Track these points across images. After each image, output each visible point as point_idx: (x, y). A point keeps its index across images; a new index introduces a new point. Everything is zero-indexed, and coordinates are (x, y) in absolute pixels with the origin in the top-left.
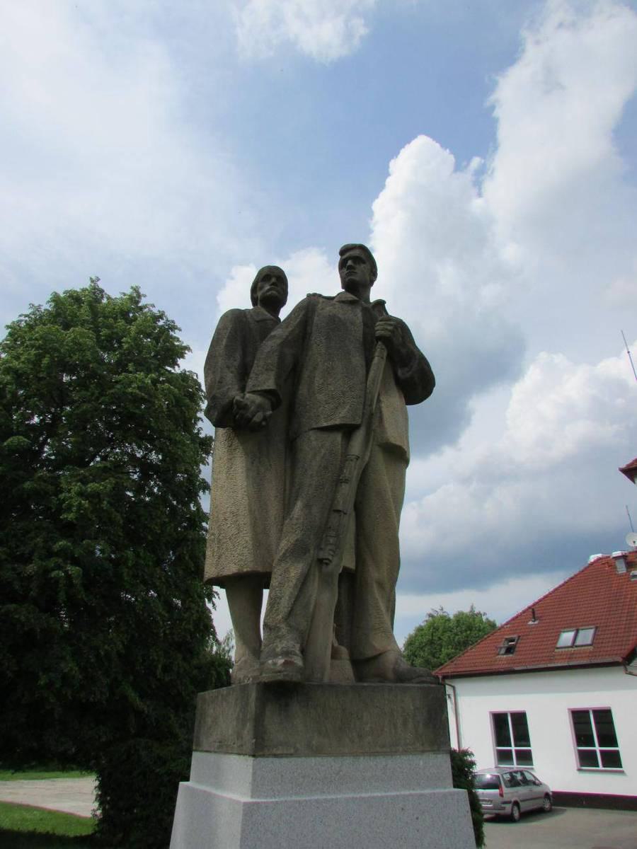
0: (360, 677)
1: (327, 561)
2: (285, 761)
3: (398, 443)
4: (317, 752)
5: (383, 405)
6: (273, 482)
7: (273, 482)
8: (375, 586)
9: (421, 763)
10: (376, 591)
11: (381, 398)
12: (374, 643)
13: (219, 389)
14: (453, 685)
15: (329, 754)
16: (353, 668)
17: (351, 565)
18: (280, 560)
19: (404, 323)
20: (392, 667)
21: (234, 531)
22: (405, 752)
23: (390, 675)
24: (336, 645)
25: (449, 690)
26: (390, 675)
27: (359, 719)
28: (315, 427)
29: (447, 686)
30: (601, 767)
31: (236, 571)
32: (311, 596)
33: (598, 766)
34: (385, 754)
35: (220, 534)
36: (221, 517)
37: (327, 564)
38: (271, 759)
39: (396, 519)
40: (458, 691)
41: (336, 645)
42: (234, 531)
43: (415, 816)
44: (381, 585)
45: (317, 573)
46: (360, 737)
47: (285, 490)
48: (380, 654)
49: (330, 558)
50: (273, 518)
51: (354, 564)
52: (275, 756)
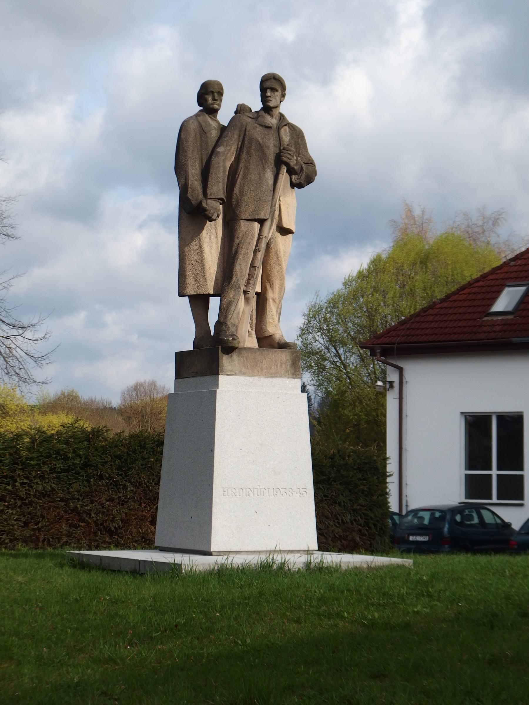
0: (260, 345)
2: (231, 377)
4: (244, 374)
11: (281, 199)
15: (249, 375)
16: (310, 157)
17: (259, 291)
22: (281, 377)
23: (276, 345)
24: (250, 330)
30: (495, 500)
33: (490, 498)
34: (272, 377)
38: (226, 376)
45: (243, 297)
46: (262, 370)
52: (227, 375)
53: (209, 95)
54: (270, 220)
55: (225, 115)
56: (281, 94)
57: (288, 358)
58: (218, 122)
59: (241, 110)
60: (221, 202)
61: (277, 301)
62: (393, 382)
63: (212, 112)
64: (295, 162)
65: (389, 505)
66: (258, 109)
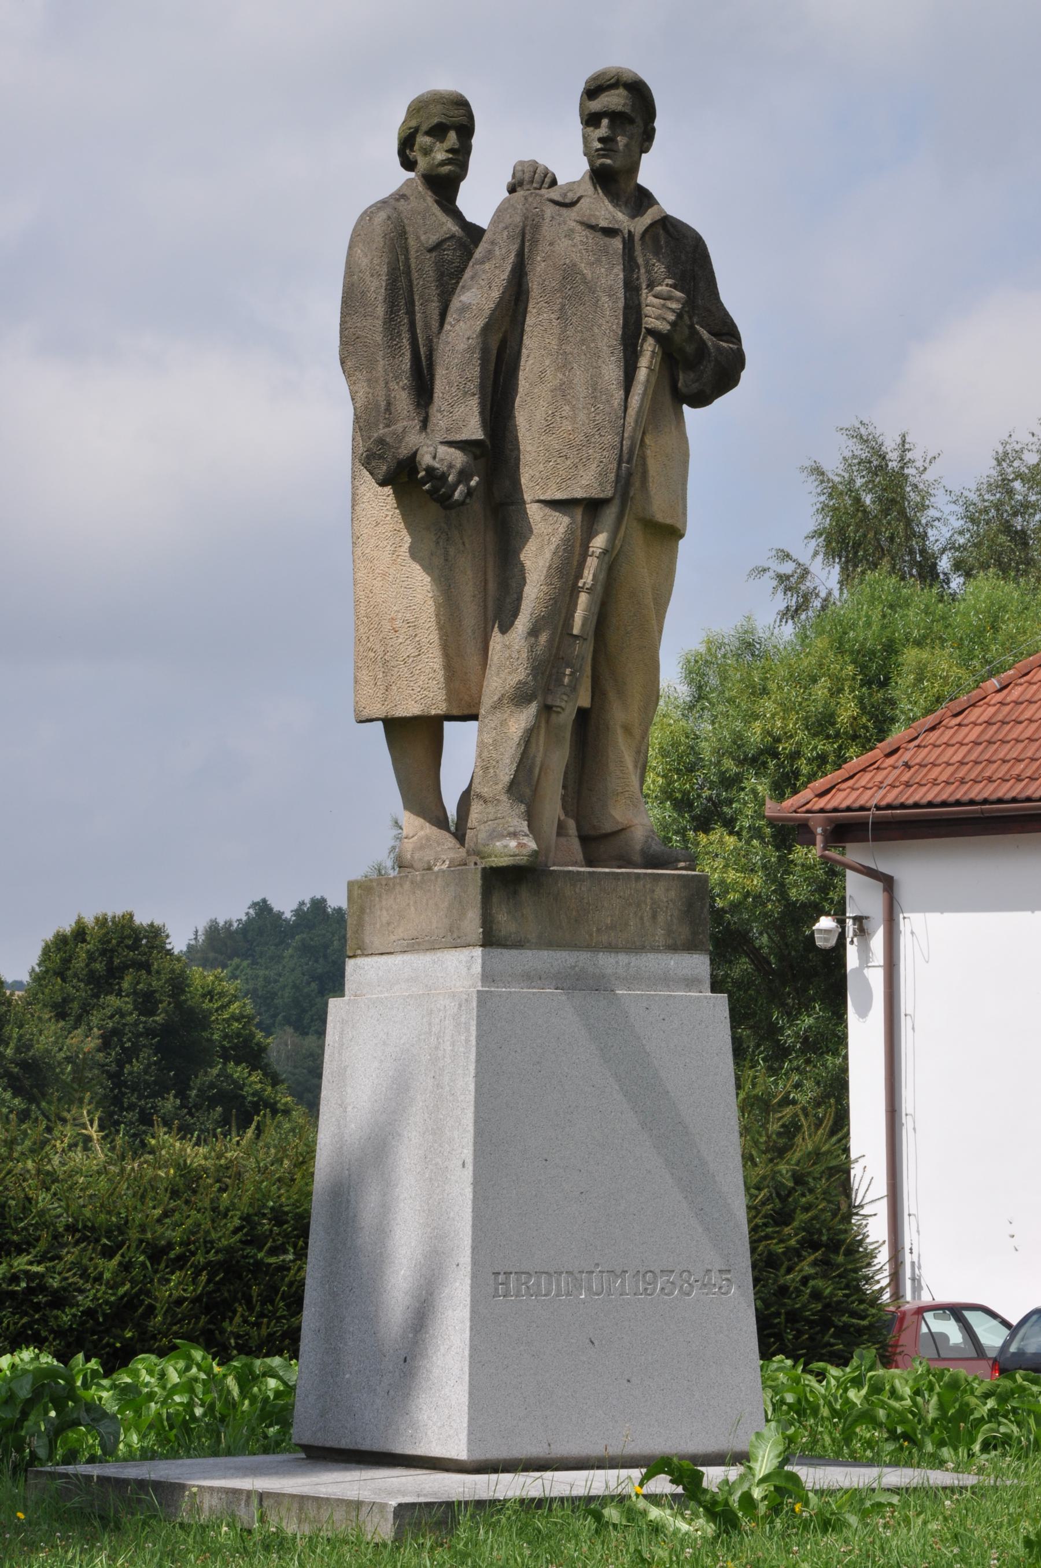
1: (559, 709)
3: (669, 521)
5: (648, 452)
6: (469, 572)
7: (469, 572)
8: (619, 731)
9: (672, 963)
10: (620, 740)
11: (647, 441)
12: (613, 813)
13: (388, 426)
14: (884, 868)
18: (494, 708)
19: (701, 238)
20: (638, 847)
21: (411, 650)
23: (637, 858)
24: (562, 818)
25: (861, 895)
26: (637, 858)
27: (864, 747)
28: (542, 498)
29: (852, 878)
31: (419, 713)
32: (535, 757)
35: (385, 653)
36: (387, 626)
37: (559, 713)
39: (657, 634)
40: (905, 891)
41: (562, 818)
42: (411, 650)
43: (662, 1017)
44: (627, 730)
47: (486, 582)
48: (623, 829)
49: (563, 704)
50: (469, 631)
51: (589, 700)
53: (439, 135)
54: (617, 502)
55: (481, 198)
56: (641, 130)
57: (672, 894)
58: (457, 215)
59: (531, 180)
60: (478, 452)
61: (637, 732)
62: (867, 918)
63: (444, 186)
64: (687, 331)
65: (221, 923)
66: (577, 177)
